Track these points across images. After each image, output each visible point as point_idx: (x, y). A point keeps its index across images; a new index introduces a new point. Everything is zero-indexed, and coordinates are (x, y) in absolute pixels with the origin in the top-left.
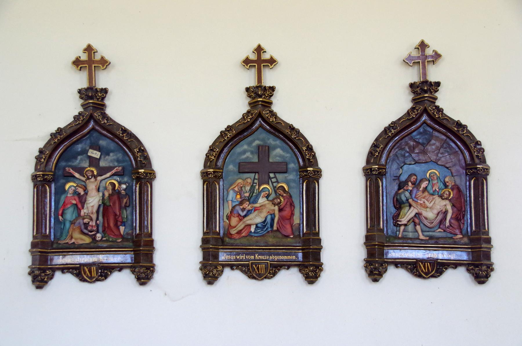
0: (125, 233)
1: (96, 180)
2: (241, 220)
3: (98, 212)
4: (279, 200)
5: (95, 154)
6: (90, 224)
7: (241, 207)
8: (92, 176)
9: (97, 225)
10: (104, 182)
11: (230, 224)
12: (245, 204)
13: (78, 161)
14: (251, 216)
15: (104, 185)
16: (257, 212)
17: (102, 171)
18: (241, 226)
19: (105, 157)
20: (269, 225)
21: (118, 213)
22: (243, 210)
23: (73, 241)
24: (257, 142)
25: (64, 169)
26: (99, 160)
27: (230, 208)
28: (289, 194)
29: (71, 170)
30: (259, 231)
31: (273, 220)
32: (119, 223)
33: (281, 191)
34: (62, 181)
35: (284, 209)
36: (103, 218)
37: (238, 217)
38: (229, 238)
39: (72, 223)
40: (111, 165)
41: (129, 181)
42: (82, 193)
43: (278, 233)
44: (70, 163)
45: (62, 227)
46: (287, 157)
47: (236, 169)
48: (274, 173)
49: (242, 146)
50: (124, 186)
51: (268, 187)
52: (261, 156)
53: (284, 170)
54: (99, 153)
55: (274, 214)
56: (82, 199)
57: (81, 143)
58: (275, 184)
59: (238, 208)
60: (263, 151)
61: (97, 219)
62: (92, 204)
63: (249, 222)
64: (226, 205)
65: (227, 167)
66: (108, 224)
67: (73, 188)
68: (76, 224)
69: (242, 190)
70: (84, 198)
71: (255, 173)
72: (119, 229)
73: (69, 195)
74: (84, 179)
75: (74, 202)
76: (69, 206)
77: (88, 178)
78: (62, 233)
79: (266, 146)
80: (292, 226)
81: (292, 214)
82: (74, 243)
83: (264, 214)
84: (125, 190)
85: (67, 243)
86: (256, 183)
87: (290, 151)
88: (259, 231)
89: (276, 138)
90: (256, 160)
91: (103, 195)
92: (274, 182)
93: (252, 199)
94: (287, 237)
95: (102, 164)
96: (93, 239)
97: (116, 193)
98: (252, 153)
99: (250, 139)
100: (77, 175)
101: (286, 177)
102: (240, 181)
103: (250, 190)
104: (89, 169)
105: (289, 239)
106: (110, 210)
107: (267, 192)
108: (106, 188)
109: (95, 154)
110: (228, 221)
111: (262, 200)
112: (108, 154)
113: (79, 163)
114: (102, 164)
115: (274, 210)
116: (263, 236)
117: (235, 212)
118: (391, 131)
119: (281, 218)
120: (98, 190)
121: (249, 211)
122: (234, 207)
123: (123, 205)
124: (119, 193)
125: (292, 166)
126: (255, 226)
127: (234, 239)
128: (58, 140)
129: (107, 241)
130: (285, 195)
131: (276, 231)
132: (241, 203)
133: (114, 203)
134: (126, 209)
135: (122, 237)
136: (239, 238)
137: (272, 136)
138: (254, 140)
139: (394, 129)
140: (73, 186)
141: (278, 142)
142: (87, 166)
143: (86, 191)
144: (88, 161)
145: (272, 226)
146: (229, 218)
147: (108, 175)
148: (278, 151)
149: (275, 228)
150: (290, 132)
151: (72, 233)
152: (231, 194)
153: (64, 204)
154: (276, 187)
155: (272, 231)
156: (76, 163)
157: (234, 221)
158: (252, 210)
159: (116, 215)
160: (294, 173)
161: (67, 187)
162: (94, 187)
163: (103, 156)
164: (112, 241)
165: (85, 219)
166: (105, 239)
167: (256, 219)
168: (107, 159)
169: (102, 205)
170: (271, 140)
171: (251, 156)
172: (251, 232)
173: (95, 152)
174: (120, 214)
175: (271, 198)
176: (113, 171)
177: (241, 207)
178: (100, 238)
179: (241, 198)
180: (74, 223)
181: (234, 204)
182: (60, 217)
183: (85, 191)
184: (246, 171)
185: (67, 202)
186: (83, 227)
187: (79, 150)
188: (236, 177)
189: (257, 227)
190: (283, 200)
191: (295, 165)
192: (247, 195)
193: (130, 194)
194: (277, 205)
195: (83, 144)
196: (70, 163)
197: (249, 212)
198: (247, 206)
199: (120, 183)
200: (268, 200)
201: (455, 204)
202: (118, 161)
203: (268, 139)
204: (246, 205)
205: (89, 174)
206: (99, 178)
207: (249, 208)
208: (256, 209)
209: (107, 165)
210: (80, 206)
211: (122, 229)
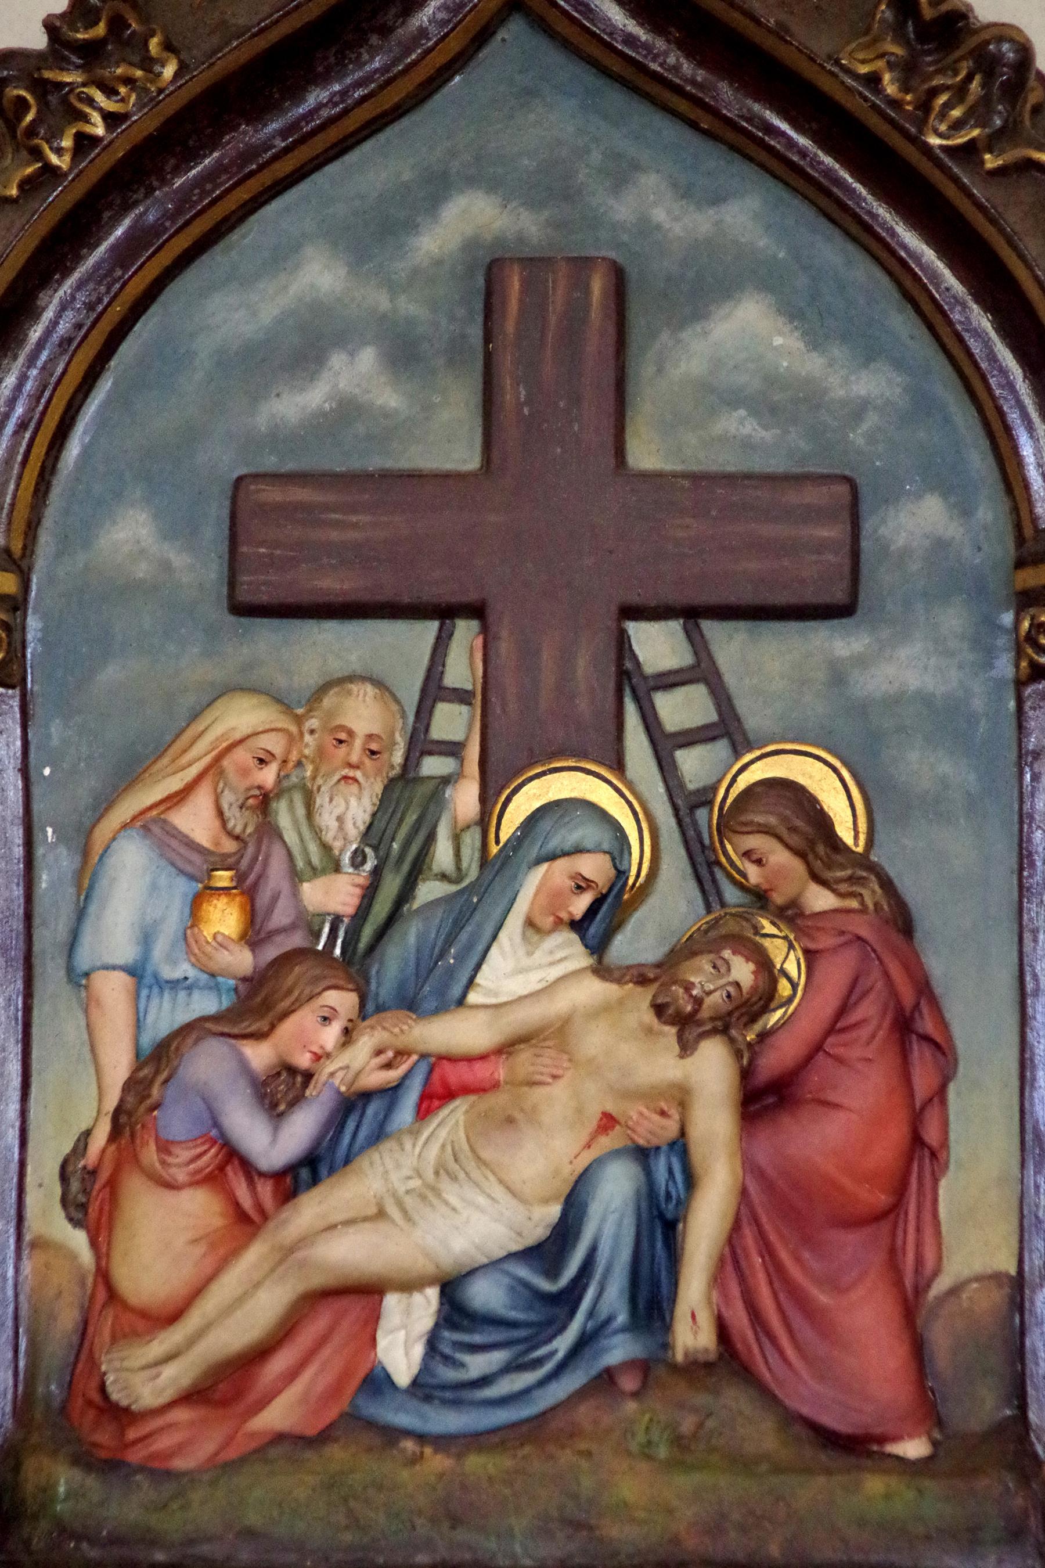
2: (246, 1223)
4: (743, 971)
7: (259, 1055)
11: (103, 1274)
12: (305, 1018)
14: (381, 1173)
16: (454, 1116)
18: (246, 1304)
20: (611, 1295)
22: (281, 1089)
24: (471, 216)
27: (119, 1064)
28: (872, 893)
30: (478, 1364)
31: (661, 1223)
33: (779, 857)
35: (813, 1079)
37: (212, 1178)
38: (85, 1459)
43: (735, 1399)
46: (859, 410)
47: (196, 569)
48: (691, 615)
49: (283, 257)
51: (602, 794)
52: (512, 393)
53: (814, 576)
55: (680, 1145)
58: (695, 765)
59: (208, 1065)
60: (555, 334)
63: (350, 1253)
64: (58, 1018)
65: (80, 535)
69: (268, 830)
71: (446, 613)
79: (582, 265)
80: (911, 1309)
81: (922, 1152)
83: (546, 1153)
86: (454, 749)
87: (902, 324)
88: (478, 1364)
89: (713, 159)
90: (451, 443)
92: (690, 738)
93: (396, 945)
94: (855, 1447)
98: (404, 353)
99: (374, 170)
101: (838, 676)
102: (242, 717)
103: (373, 835)
105: (874, 1484)
107: (594, 867)
110: (78, 1240)
111: (524, 971)
115: (681, 1097)
116: (535, 1431)
117: (176, 1121)
119: (775, 1205)
121: (352, 1103)
122: (158, 1060)
125: (915, 523)
126: (426, 1304)
127: (160, 1473)
128: (84, 143)
130: (820, 899)
131: (697, 1370)
132: (257, 1003)
136: (224, 1468)
137: (670, 131)
138: (436, 187)
141: (746, 215)
145: (652, 1302)
146: (92, 1196)
148: (750, 330)
149: (692, 1333)
150: (908, 71)
152: (132, 895)
154: (704, 797)
155: (654, 1368)
157: (163, 1232)
158: (392, 1093)
160: (954, 619)
167: (448, 1208)
170: (650, 181)
171: (389, 398)
172: (378, 1382)
175: (638, 942)
177: (259, 1055)
179: (253, 934)
181: (166, 1016)
184: (334, 584)
188: (196, 668)
189: (455, 1312)
190: (792, 964)
191: (965, 511)
192: (335, 894)
194: (721, 1026)
197: (357, 1120)
198: (329, 1038)
200: (601, 971)
203: (620, 174)
204: (320, 1031)
207: (359, 1063)
208: (442, 1084)
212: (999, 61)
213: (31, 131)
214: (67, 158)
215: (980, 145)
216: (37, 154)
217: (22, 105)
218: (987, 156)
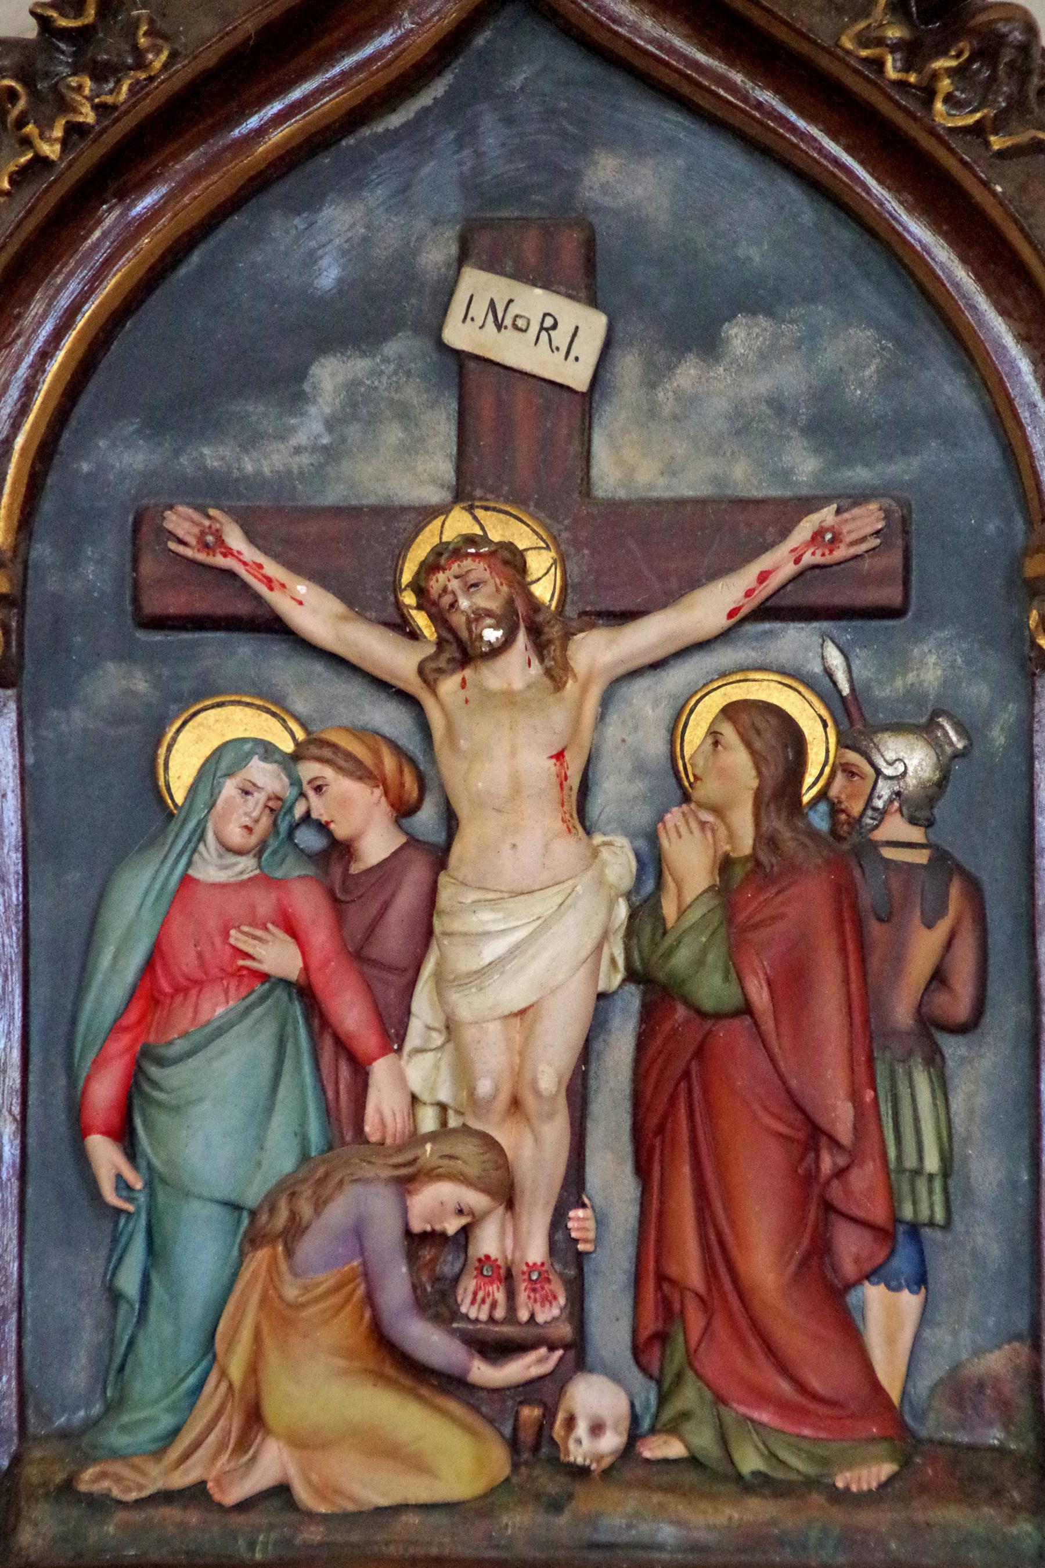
0: (932, 1373)
1: (557, 675)
3: (578, 1093)
5: (537, 331)
6: (489, 1242)
8: (509, 623)
9: (570, 1259)
10: (647, 703)
13: (310, 427)
15: (656, 746)
17: (635, 559)
19: (654, 376)
21: (841, 1116)
23: (272, 1462)
25: (143, 527)
26: (586, 404)
29: (235, 539)
32: (850, 1245)
34: (119, 683)
36: (642, 1170)
39: (261, 1227)
40: (743, 476)
41: (978, 692)
42: (377, 844)
44: (214, 455)
45: (129, 1282)
50: (909, 760)
54: (594, 325)
56: (374, 926)
57: (351, 182)
61: (574, 1186)
62: (512, 993)
66: (720, 1254)
67: (265, 775)
68: (309, 1247)
70: (407, 898)
72: (849, 1330)
73: (210, 869)
74: (398, 659)
75: (279, 957)
76: (216, 1007)
77: (462, 652)
78: (115, 1370)
82: (282, 1491)
84: (921, 807)
85: (197, 1495)
91: (652, 863)
95: (625, 462)
96: (514, 1444)
97: (808, 857)
100: (310, 608)
104: (459, 524)
106: (743, 1072)
108: (678, 785)
109: (537, 331)
112: (696, 334)
113: (331, 454)
114: (625, 462)
118: (64, 106)
120: (581, 806)
123: (902, 1012)
124: (848, 843)
128: (76, 131)
129: (706, 1475)
133: (793, 983)
134: (934, 1059)
135: (891, 1422)
139: (101, 73)
140: (267, 750)
142: (435, 496)
143: (427, 818)
144: (441, 427)
147: (710, 607)
151: (254, 1369)
153: (157, 988)
156: (284, 449)
159: (814, 1134)
161: (183, 763)
162: (536, 764)
163: (629, 366)
164: (761, 1485)
165: (432, 1175)
166: (675, 1449)
168: (689, 402)
169: (633, 999)
173: (534, 301)
174: (865, 1116)
176: (780, 562)
178: (611, 1442)
180: (294, 1232)
182: (105, 1154)
183: (403, 811)
185: (185, 960)
186: (396, 1285)
187: (329, 275)
193: (993, 869)
195: (377, 195)
196: (214, 455)
199: (856, 720)
201: (233, 1422)
202: (830, 425)
205: (475, 595)
206: (597, 651)
209: (692, 483)
210: (351, 1014)
211: (888, 1315)
212: (997, 49)
213: (21, 122)
214: (58, 147)
215: (988, 123)
216: (26, 142)
217: (12, 95)
218: (992, 138)
